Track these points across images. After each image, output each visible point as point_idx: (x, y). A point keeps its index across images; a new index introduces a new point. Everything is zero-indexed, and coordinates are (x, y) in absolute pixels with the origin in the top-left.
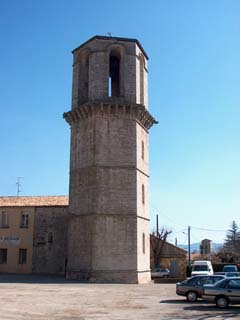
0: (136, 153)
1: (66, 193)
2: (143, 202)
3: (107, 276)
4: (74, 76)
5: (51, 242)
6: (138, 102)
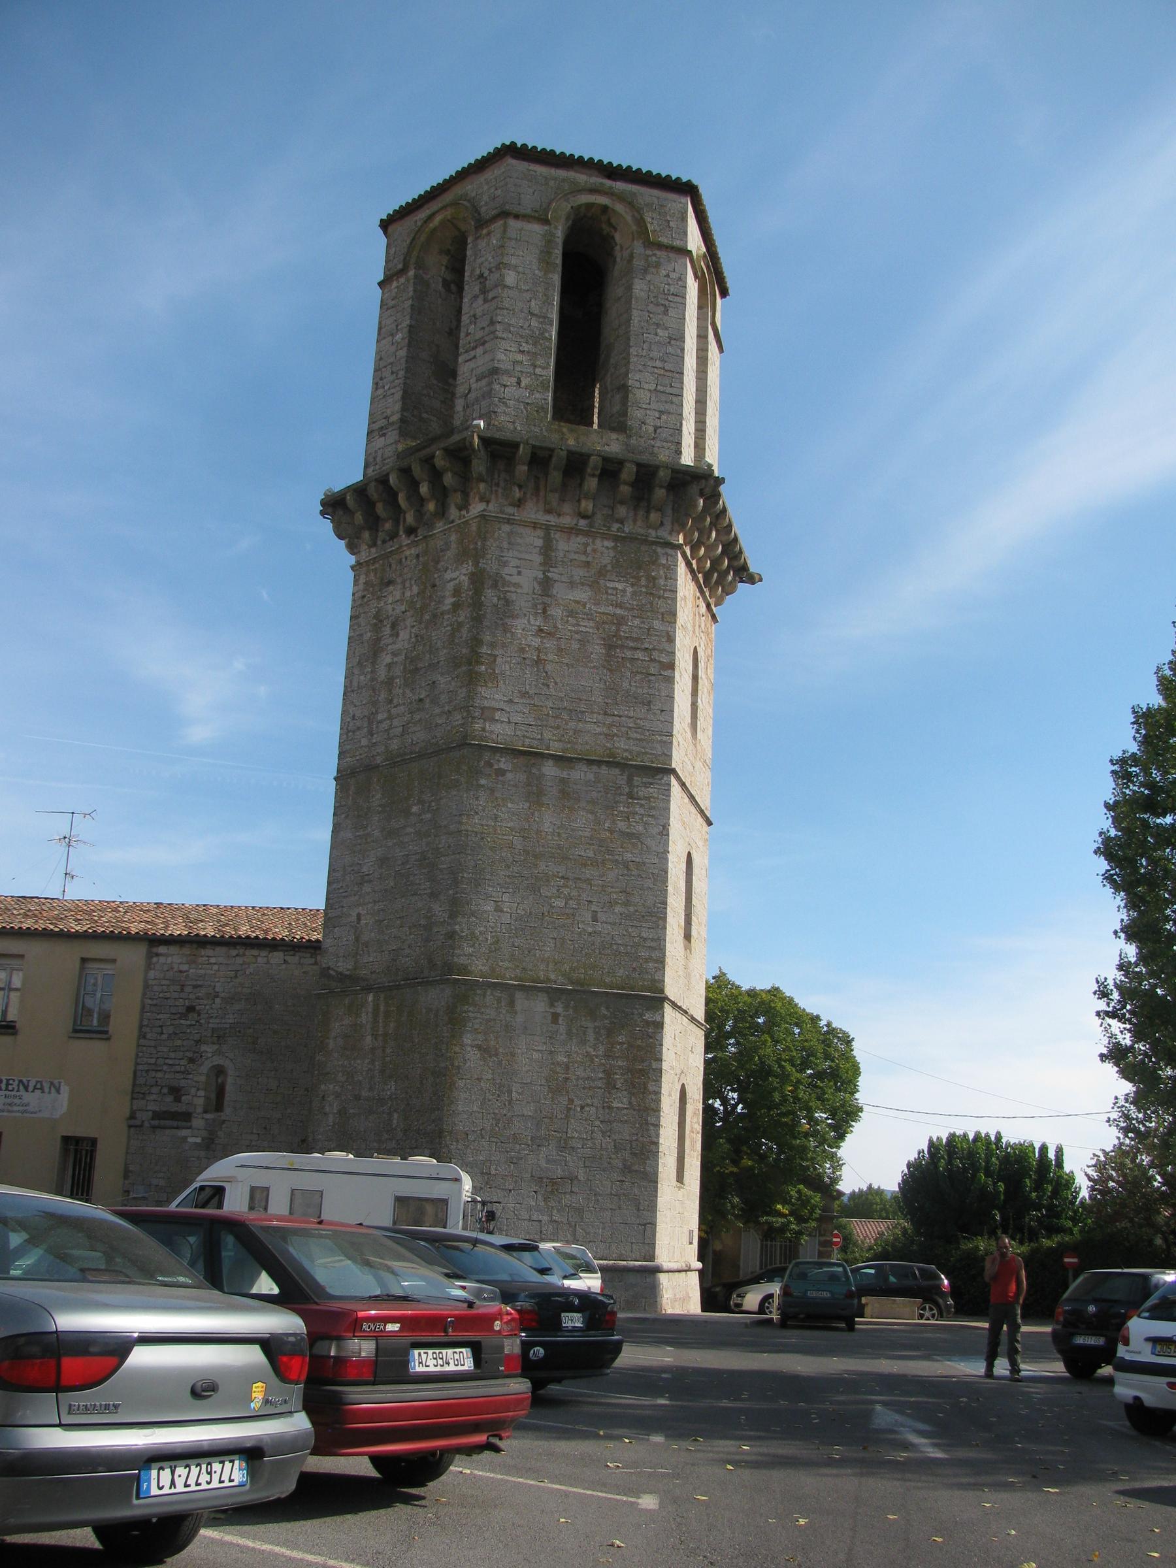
0: (671, 697)
2: (688, 937)
3: (222, 1516)
5: (218, 1102)
6: (687, 458)
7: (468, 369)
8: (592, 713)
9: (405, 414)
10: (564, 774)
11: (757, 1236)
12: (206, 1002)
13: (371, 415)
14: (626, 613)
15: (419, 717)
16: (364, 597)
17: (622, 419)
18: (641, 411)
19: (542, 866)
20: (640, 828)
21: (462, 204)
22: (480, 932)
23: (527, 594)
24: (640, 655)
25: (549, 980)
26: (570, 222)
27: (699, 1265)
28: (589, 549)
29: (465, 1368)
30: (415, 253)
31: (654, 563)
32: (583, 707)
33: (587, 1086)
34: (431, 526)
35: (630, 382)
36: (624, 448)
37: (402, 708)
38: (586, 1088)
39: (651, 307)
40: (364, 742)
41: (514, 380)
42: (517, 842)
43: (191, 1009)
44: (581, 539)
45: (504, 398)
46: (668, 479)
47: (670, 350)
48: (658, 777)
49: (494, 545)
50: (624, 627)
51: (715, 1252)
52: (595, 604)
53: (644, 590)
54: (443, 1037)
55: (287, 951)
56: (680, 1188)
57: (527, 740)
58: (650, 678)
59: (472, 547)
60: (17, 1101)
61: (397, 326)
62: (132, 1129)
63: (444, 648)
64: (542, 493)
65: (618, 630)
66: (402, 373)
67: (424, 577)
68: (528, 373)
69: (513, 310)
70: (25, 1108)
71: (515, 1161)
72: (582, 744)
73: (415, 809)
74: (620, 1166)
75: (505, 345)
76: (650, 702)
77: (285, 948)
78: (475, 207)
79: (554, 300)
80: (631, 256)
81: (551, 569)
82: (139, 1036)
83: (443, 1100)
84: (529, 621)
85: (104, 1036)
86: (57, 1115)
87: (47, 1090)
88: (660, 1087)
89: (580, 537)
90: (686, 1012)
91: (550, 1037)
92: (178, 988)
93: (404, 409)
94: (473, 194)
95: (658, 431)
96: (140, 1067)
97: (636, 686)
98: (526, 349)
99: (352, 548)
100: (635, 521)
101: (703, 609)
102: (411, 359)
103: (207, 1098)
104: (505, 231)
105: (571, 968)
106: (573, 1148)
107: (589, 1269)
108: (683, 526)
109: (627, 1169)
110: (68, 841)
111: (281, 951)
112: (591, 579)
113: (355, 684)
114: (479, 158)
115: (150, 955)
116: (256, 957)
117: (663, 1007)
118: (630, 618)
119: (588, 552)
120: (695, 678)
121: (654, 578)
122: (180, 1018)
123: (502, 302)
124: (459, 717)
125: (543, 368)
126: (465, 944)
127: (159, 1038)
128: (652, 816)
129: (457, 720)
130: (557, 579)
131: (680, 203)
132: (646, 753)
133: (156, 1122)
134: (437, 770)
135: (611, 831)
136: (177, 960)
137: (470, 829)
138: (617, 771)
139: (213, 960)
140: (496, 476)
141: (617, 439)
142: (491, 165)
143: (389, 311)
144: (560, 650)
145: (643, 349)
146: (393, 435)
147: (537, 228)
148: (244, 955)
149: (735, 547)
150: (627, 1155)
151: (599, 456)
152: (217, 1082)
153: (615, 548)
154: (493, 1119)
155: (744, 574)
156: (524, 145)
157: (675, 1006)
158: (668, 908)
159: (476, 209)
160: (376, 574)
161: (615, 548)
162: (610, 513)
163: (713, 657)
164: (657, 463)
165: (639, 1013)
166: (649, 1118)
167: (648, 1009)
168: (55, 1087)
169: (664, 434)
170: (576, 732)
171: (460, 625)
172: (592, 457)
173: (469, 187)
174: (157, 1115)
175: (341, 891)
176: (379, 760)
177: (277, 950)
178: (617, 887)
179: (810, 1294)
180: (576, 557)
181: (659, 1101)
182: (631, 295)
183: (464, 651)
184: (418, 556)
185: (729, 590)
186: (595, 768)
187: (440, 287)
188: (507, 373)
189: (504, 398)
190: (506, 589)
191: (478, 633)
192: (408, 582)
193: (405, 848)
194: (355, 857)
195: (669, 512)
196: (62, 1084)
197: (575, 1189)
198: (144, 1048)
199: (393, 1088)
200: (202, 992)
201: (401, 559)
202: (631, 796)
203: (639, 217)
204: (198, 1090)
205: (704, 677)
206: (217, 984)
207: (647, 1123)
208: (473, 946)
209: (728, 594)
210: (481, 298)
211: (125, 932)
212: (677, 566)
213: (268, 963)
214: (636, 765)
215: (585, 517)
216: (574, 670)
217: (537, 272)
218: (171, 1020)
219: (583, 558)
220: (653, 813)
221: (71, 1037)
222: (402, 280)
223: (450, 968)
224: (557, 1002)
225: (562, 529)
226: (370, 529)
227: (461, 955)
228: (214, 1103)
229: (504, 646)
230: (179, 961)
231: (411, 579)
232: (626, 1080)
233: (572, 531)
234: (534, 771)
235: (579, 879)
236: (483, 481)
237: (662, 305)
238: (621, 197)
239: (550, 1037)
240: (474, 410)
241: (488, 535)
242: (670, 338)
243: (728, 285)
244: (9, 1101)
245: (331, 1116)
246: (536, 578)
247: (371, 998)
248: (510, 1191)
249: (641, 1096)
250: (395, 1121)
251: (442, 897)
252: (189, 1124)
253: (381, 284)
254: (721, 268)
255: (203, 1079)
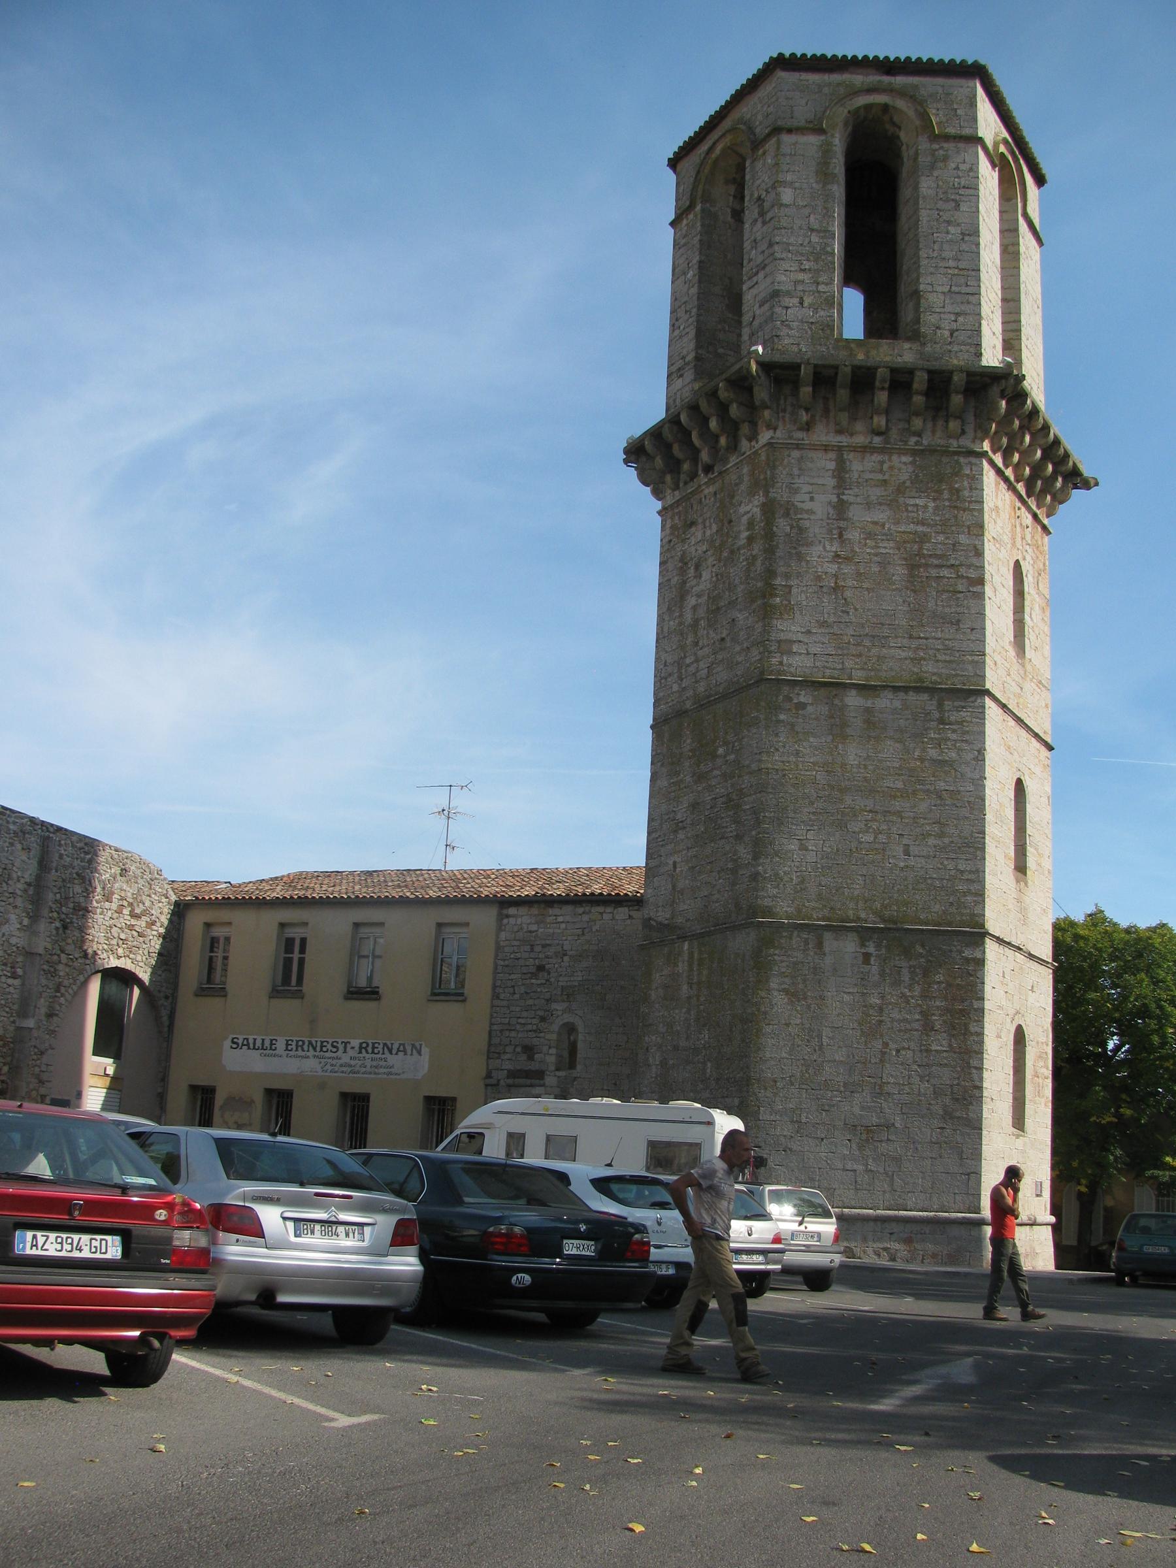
1: (640, 840)
2: (1021, 868)
4: (677, 273)
7: (750, 297)
8: (896, 637)
9: (700, 351)
10: (869, 704)
11: (1152, 1191)
12: (554, 961)
13: (670, 357)
14: (929, 530)
15: (721, 657)
16: (670, 541)
17: (916, 327)
18: (935, 316)
19: (848, 800)
20: (954, 755)
21: (739, 128)
22: (785, 873)
23: (822, 520)
24: (945, 572)
25: (859, 919)
26: (850, 128)
27: (1053, 1219)
28: (885, 467)
29: (108, 1256)
30: (701, 187)
31: (957, 474)
32: (886, 631)
33: (903, 1028)
34: (725, 460)
35: (922, 287)
36: (918, 356)
37: (706, 649)
38: (903, 1031)
39: (940, 204)
40: (675, 688)
41: (796, 301)
42: (821, 777)
43: (541, 968)
44: (876, 457)
45: (787, 321)
46: (963, 383)
47: (964, 247)
48: (970, 700)
49: (784, 472)
50: (927, 544)
51: (1106, 1209)
52: (894, 524)
53: (947, 503)
54: (749, 982)
55: (631, 906)
56: (1018, 1137)
57: (828, 671)
58: (958, 595)
59: (762, 477)
60: (382, 1063)
61: (688, 264)
62: (489, 1088)
63: (741, 583)
64: (832, 414)
65: (921, 548)
66: (695, 310)
67: (721, 514)
68: (810, 291)
69: (792, 228)
70: (391, 1070)
71: (827, 1108)
72: (886, 671)
73: (721, 751)
74: (941, 1112)
75: (785, 265)
76: (959, 621)
77: (629, 904)
78: (750, 128)
79: (834, 212)
80: (917, 154)
81: (846, 492)
82: (493, 996)
83: (749, 1047)
84: (824, 547)
85: (461, 998)
86: (420, 1075)
87: (409, 1052)
88: (983, 1028)
89: (875, 455)
90: (1020, 949)
91: (862, 979)
92: (528, 948)
93: (698, 346)
94: (749, 116)
95: (954, 335)
96: (495, 1027)
97: (943, 606)
98: (807, 267)
99: (657, 493)
100: (934, 432)
101: (1028, 519)
102: (703, 296)
103: (559, 1056)
104: (778, 148)
105: (882, 905)
106: (889, 1094)
107: (826, 1214)
108: (985, 434)
109: (948, 1115)
110: (446, 813)
111: (626, 906)
112: (889, 498)
113: (666, 630)
114: (750, 77)
115: (501, 917)
116: (601, 914)
117: (983, 943)
118: (933, 534)
119: (884, 470)
120: (1019, 594)
121: (958, 491)
122: (531, 978)
123: (779, 221)
124: (756, 652)
125: (827, 284)
126: (769, 886)
127: (511, 998)
128: (966, 741)
129: (755, 656)
130: (852, 501)
131: (968, 87)
132: (957, 675)
133: (510, 1081)
134: (739, 709)
135: (922, 760)
136: (526, 920)
137: (770, 766)
138: (925, 696)
139: (560, 919)
140: (782, 402)
141: (911, 348)
142: (763, 82)
143: (681, 250)
144: (859, 574)
145: (934, 250)
146: (689, 375)
147: (813, 139)
148: (590, 912)
149: (1058, 451)
150: (947, 1101)
151: (887, 367)
152: (569, 1038)
153: (913, 463)
154: (802, 1065)
155: (1076, 479)
156: (793, 55)
157: (1000, 941)
158: (987, 837)
159: (751, 130)
160: (680, 517)
161: (913, 463)
162: (907, 426)
163: (1047, 571)
164: (950, 368)
165: (957, 951)
166: (971, 1061)
167: (967, 946)
168: (416, 1048)
169: (962, 336)
170: (880, 658)
171: (754, 558)
172: (879, 370)
173: (744, 110)
174: (512, 1074)
175: (659, 840)
176: (688, 705)
177: (622, 906)
178: (930, 819)
179: (1146, 1249)
180: (871, 476)
181: (981, 1043)
182: (918, 195)
183: (759, 584)
184: (715, 493)
185: (1060, 498)
186: (901, 695)
187: (729, 219)
188: (789, 294)
189: (787, 321)
190: (799, 516)
191: (771, 565)
192: (708, 521)
193: (713, 791)
194: (670, 804)
195: (970, 417)
196: (423, 1046)
197: (892, 1137)
198: (498, 1009)
199: (707, 1037)
200: (550, 951)
201: (701, 499)
202: (942, 721)
203: (922, 111)
204: (550, 1048)
205: (1033, 592)
206: (565, 942)
207: (970, 1067)
208: (778, 887)
209: (1061, 503)
210: (760, 220)
211: (475, 896)
212: (982, 475)
213: (613, 918)
214: (945, 689)
215: (879, 434)
216: (875, 595)
217: (814, 185)
218: (522, 979)
219: (880, 477)
220: (967, 737)
221: (429, 1000)
222: (691, 216)
223: (754, 911)
224: (869, 941)
225: (854, 449)
226: (671, 472)
227: (765, 897)
228: (567, 1060)
229: (799, 575)
230: (529, 921)
231: (710, 518)
232: (945, 1022)
233: (865, 450)
234: (836, 702)
235: (889, 812)
236: (767, 407)
237: (953, 200)
238: (901, 93)
239: (862, 979)
240: (758, 337)
241: (777, 463)
242: (962, 234)
243: (1044, 172)
244: (375, 1063)
245: (654, 1067)
246: (830, 503)
247: (686, 946)
248: (822, 1139)
249: (962, 1037)
250: (708, 1071)
251: (746, 839)
252: (542, 1082)
253: (672, 224)
254: (1032, 153)
255: (554, 1036)
